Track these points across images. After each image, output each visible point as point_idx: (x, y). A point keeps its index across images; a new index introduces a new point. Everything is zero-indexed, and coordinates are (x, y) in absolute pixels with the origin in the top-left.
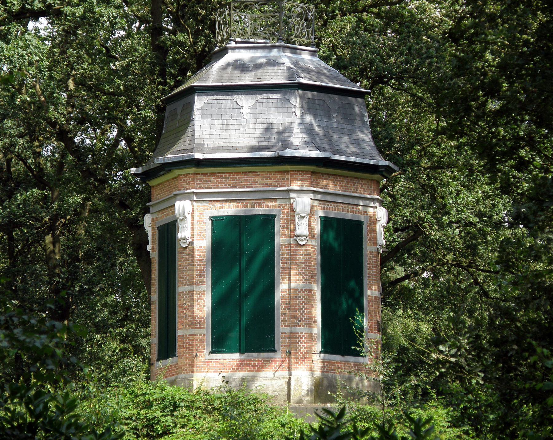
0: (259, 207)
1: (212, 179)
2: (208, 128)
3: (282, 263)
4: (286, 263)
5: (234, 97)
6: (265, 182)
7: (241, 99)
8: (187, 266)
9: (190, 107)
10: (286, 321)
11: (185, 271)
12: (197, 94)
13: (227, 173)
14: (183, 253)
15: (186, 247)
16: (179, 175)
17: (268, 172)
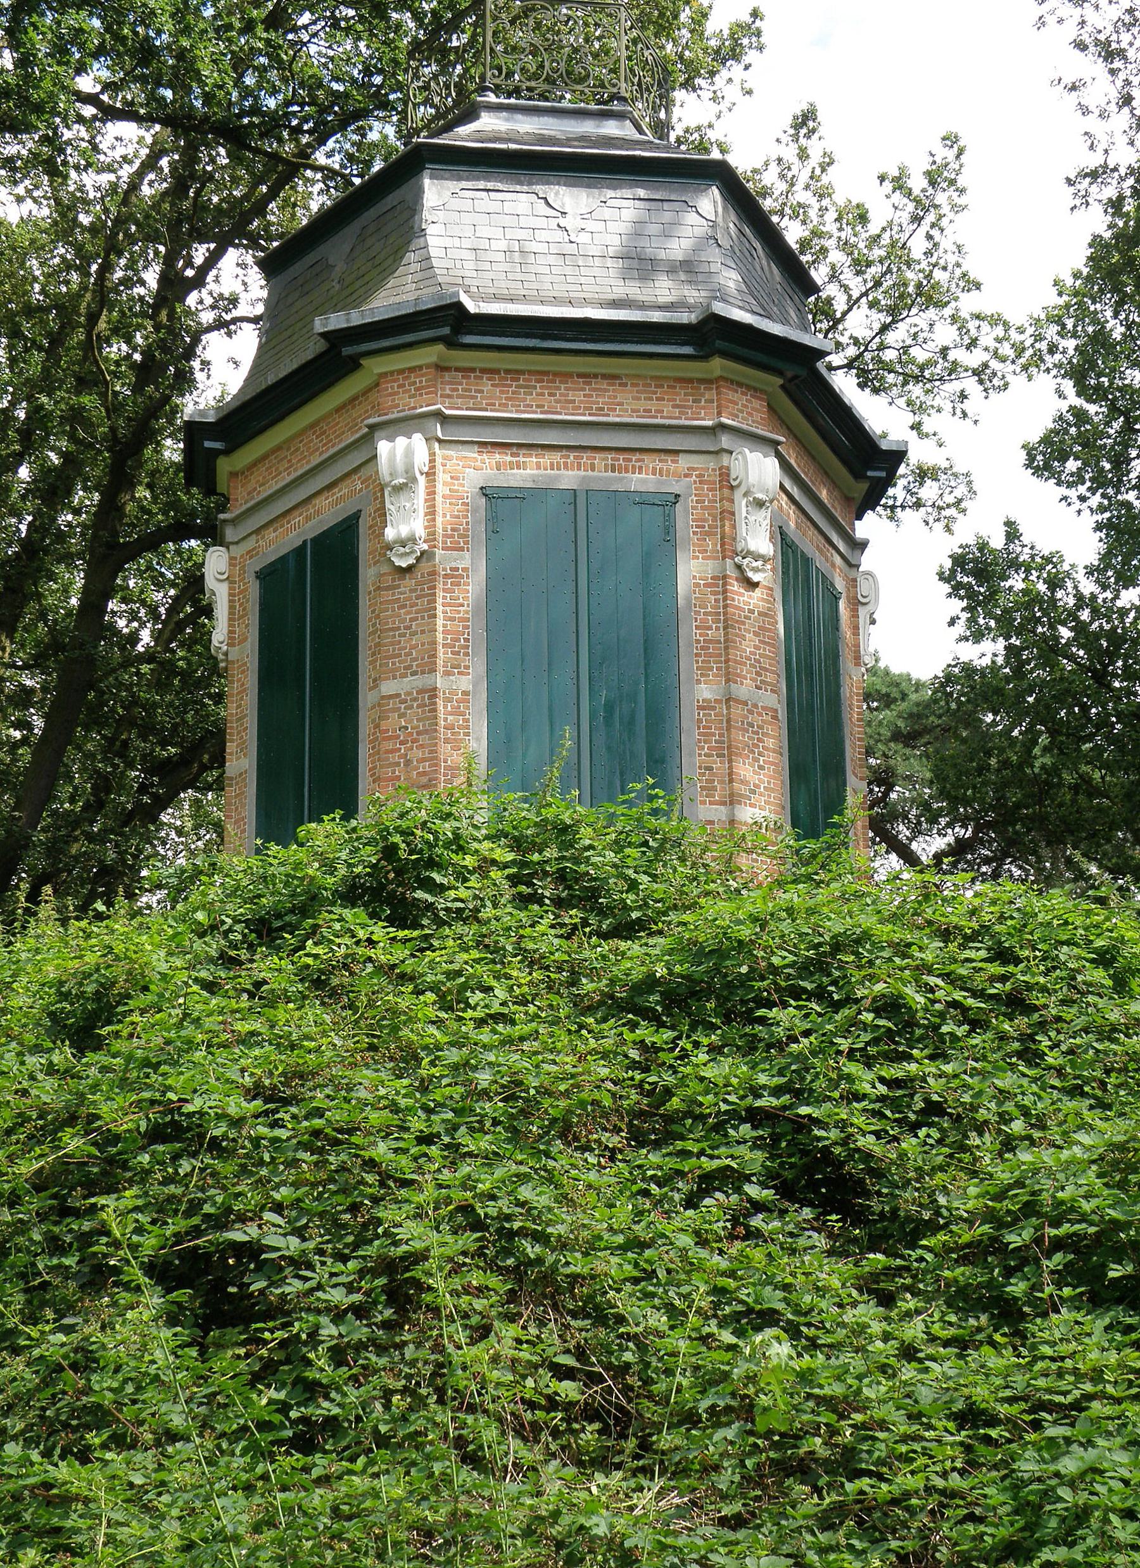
1: (487, 386)
2: (470, 255)
5: (538, 188)
6: (642, 405)
9: (413, 207)
10: (714, 789)
12: (426, 173)
13: (530, 372)
15: (410, 569)
16: (385, 375)
17: (652, 378)
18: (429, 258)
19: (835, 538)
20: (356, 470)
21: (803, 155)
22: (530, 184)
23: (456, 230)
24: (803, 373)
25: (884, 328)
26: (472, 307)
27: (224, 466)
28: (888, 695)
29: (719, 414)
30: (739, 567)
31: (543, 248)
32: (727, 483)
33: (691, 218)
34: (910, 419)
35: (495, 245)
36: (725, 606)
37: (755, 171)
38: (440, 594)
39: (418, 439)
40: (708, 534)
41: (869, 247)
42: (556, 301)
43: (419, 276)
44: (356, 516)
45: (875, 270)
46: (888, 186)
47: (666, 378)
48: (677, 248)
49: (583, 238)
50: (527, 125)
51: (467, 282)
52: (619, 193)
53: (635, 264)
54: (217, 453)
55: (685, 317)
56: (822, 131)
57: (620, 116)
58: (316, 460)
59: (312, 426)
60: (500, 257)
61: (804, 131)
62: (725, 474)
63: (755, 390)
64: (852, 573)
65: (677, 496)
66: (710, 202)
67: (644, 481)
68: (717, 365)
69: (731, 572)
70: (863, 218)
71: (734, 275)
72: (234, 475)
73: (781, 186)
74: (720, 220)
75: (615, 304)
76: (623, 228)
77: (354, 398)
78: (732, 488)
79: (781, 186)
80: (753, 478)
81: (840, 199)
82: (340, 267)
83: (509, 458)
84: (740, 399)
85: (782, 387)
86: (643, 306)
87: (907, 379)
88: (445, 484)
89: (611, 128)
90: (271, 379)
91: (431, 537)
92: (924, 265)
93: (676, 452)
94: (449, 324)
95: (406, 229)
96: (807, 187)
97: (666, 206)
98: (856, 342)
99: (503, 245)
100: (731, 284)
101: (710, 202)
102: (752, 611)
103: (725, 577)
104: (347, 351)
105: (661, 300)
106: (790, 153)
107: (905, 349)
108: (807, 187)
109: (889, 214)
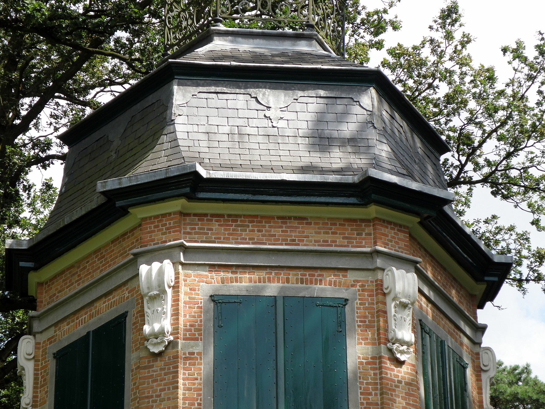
0: (311, 283)
1: (215, 226)
2: (204, 137)
3: (362, 394)
4: (370, 394)
5: (251, 91)
6: (322, 237)
7: (264, 94)
8: (161, 390)
11: (155, 401)
12: (175, 81)
14: (152, 366)
15: (161, 354)
18: (176, 140)
19: (462, 325)
20: (125, 284)
21: (449, 36)
22: (246, 88)
23: (195, 120)
24: (434, 214)
25: (509, 155)
26: (204, 173)
27: (33, 278)
28: (537, 400)
29: (375, 243)
30: (390, 350)
31: (254, 131)
32: (381, 291)
33: (356, 109)
34: (531, 217)
35: (222, 130)
36: (381, 379)
37: (415, 48)
38: (181, 372)
39: (167, 264)
40: (368, 327)
41: (497, 98)
42: (263, 168)
43: (169, 152)
44: (124, 315)
45: (501, 114)
46: (509, 56)
47: (338, 219)
48: (348, 128)
49: (282, 124)
50: (245, 47)
51: (202, 156)
52: (306, 93)
53: (317, 141)
54: (29, 269)
55: (350, 179)
56: (462, 20)
57: (309, 38)
58: (98, 275)
59: (96, 252)
60: (225, 137)
61: (449, 21)
62: (379, 285)
63: (400, 227)
64: (476, 349)
65: (346, 300)
66: (369, 98)
67: (323, 290)
68: (373, 210)
69: (385, 354)
70: (491, 79)
71: (386, 148)
72: (40, 284)
73: (433, 58)
74: (376, 111)
75: (303, 170)
76: (310, 117)
77: (125, 234)
78: (384, 294)
79: (433, 58)
80: (399, 287)
81: (475, 65)
82: (117, 142)
83: (230, 275)
84: (390, 232)
85: (420, 223)
86: (322, 171)
87: (527, 189)
88: (186, 294)
89: (303, 47)
90: (67, 220)
91: (175, 331)
92: (536, 111)
93: (346, 270)
94: (189, 185)
95: (160, 120)
96: (451, 59)
97: (339, 101)
98: (489, 163)
99: (226, 129)
100: (384, 154)
101: (369, 98)
102: (400, 382)
103: (380, 357)
104: (119, 204)
105: (335, 166)
106: (439, 36)
107: (525, 169)
108: (451, 59)
109: (511, 74)
